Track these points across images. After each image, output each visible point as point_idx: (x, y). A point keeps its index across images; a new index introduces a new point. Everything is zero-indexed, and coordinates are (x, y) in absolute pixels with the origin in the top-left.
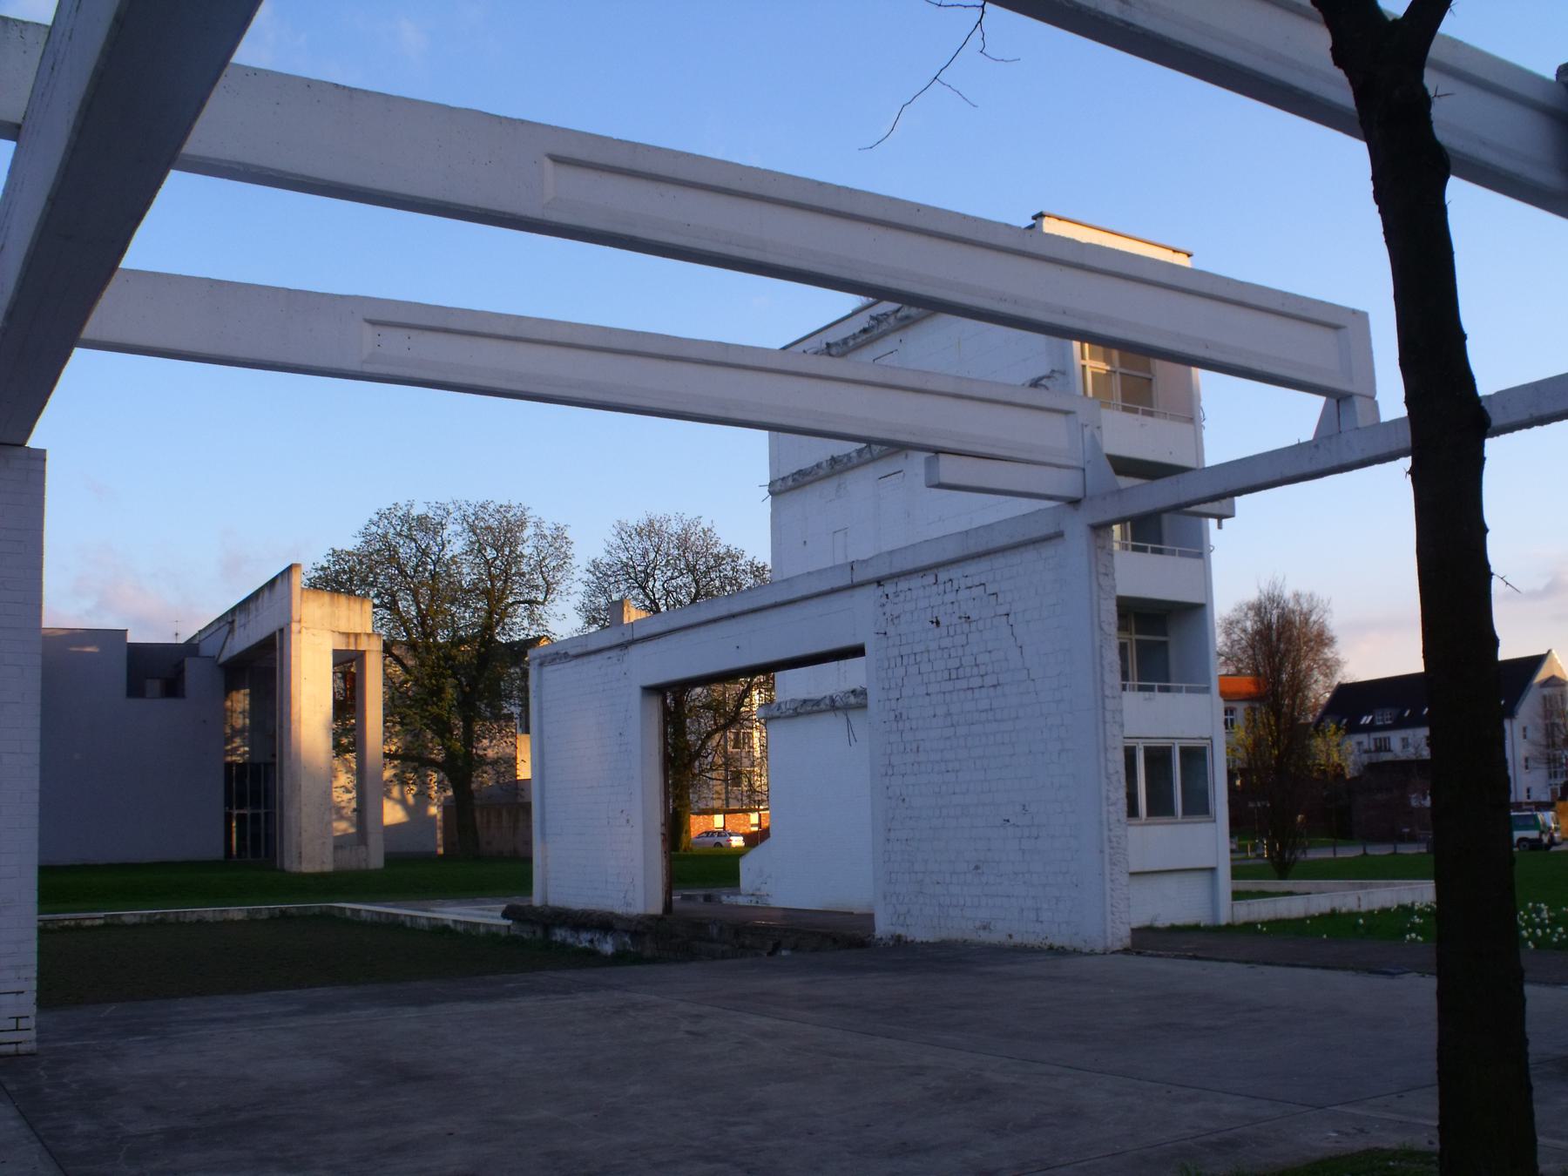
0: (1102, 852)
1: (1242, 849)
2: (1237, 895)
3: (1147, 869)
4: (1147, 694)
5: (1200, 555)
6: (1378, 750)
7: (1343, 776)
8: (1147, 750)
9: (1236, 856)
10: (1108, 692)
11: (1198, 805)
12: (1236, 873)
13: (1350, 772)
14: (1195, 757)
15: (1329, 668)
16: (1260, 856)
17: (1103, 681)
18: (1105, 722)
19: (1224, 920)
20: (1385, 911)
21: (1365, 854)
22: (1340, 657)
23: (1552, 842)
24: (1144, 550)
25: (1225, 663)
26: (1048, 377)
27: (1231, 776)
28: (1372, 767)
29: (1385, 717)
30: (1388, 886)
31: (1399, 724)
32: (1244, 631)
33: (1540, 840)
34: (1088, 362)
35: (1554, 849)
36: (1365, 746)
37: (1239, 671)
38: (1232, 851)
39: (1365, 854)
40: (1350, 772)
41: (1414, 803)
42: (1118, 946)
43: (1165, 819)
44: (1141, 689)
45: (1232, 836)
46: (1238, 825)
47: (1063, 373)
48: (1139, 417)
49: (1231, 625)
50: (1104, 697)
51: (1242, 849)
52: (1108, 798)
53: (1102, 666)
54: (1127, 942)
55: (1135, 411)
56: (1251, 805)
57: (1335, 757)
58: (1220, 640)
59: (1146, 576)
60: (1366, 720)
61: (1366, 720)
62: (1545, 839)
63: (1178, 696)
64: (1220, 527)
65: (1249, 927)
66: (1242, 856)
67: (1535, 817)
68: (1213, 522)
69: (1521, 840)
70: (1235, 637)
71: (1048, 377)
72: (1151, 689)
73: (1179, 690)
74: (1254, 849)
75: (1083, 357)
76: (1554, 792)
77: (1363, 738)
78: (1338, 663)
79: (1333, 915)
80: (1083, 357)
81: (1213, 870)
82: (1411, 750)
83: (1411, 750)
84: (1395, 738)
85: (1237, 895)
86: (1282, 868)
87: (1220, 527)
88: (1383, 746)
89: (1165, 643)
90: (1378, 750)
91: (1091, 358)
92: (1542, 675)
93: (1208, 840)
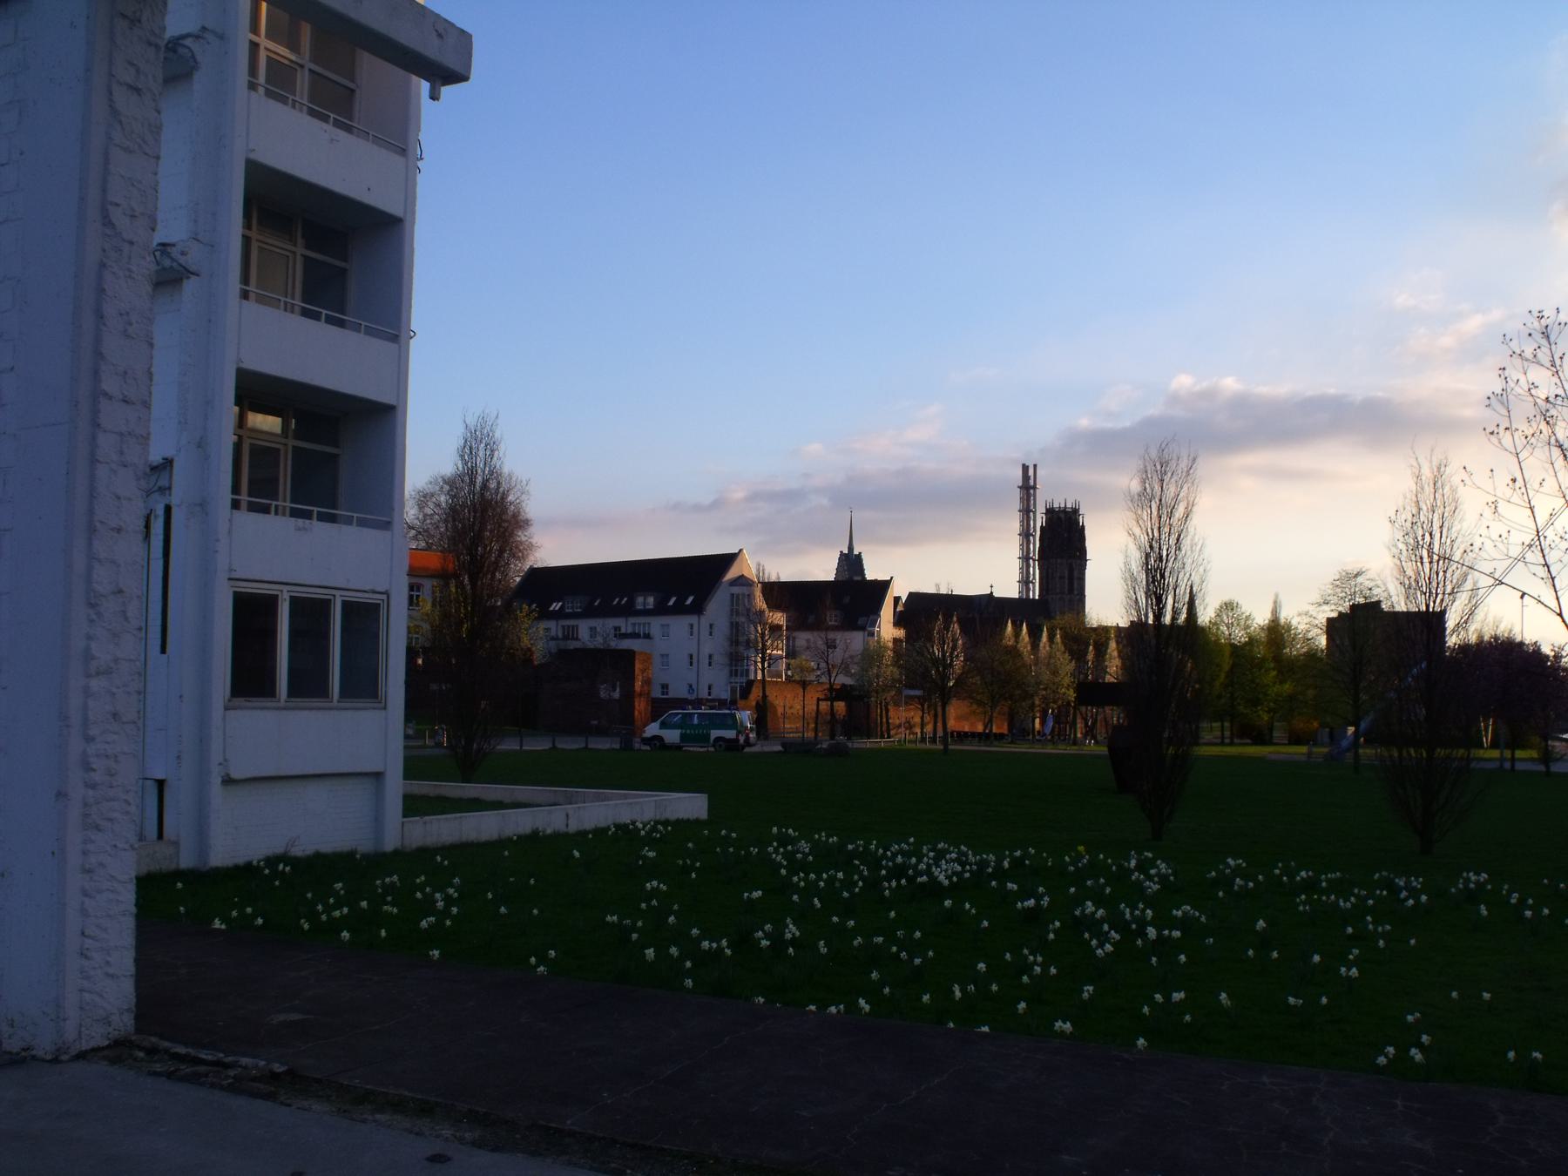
0: (61, 795)
1: (419, 735)
2: (414, 806)
3: (282, 773)
4: (300, 522)
5: (395, 338)
6: (566, 638)
7: (531, 661)
8: (295, 602)
9: (411, 743)
10: (110, 384)
11: (362, 685)
12: (413, 769)
13: (538, 658)
14: (363, 617)
15: (518, 552)
16: (439, 745)
17: (99, 355)
18: (93, 461)
19: (390, 843)
20: (600, 832)
21: (554, 747)
22: (534, 541)
23: (748, 743)
24: (315, 316)
25: (415, 538)
26: (197, 37)
27: (411, 653)
28: (563, 654)
29: (574, 605)
30: (598, 798)
31: (589, 613)
32: (438, 505)
33: (737, 740)
34: (264, 42)
35: (747, 750)
36: (553, 633)
37: (429, 548)
38: (407, 737)
39: (554, 747)
40: (538, 658)
41: (603, 694)
42: (97, 1036)
43: (315, 702)
44: (295, 514)
45: (408, 719)
46: (415, 706)
47: (221, 37)
48: (329, 127)
49: (424, 498)
50: (98, 395)
51: (419, 735)
52: (88, 656)
53: (100, 316)
54: (124, 1023)
55: (325, 119)
56: (434, 687)
57: (526, 642)
58: (411, 513)
59: (315, 354)
60: (556, 606)
61: (556, 606)
62: (742, 739)
63: (345, 528)
64: (434, 96)
65: (424, 855)
66: (420, 743)
67: (734, 716)
68: (425, 86)
69: (718, 739)
70: (429, 511)
71: (197, 37)
72: (307, 515)
73: (349, 521)
74: (434, 734)
75: (255, 29)
76: (733, 690)
77: (552, 624)
78: (531, 547)
79: (534, 837)
80: (255, 29)
81: (378, 776)
82: (600, 639)
83: (600, 639)
84: (584, 627)
85: (414, 806)
86: (468, 769)
87: (434, 96)
88: (571, 634)
89: (335, 456)
90: (566, 638)
91: (268, 36)
92: (732, 574)
93: (374, 734)
